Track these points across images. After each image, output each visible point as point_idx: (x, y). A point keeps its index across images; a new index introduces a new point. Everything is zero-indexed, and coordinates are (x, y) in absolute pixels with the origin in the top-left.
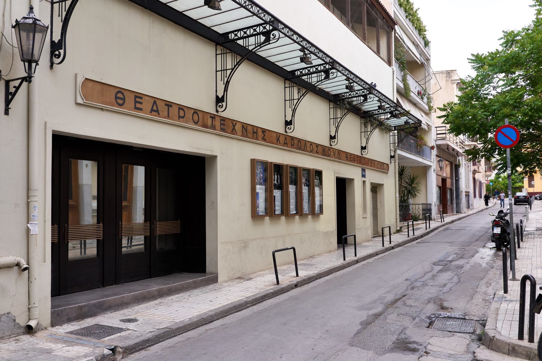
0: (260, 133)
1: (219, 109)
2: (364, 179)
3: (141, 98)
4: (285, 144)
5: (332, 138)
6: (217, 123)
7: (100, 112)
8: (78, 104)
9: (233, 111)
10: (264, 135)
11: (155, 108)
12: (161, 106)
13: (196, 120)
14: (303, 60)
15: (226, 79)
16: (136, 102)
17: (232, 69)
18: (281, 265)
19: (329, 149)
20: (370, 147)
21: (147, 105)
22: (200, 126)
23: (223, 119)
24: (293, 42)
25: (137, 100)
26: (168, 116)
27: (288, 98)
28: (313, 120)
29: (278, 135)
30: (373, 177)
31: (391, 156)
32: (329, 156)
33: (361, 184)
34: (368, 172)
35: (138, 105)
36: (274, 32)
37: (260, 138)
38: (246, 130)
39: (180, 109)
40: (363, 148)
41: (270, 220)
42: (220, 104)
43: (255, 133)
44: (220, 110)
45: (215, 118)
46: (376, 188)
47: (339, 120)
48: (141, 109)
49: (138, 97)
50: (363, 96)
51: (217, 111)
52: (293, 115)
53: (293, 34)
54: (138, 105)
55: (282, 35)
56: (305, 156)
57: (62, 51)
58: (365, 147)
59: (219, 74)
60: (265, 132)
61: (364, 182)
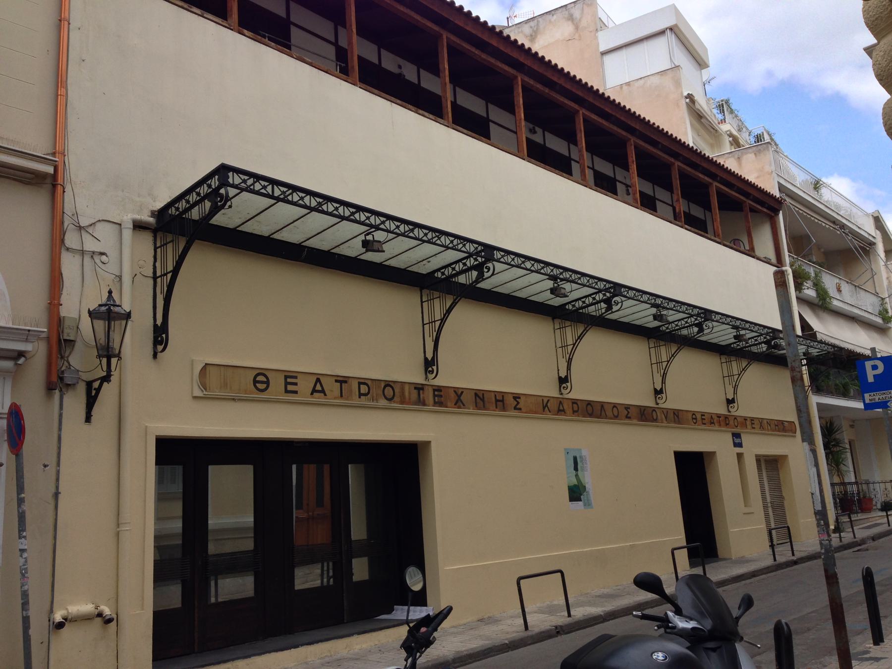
0: (510, 401)
1: (659, 401)
2: (739, 450)
5: (658, 392)
6: (429, 395)
7: (232, 403)
8: (195, 398)
9: (672, 401)
10: (518, 403)
11: (561, 408)
12: (328, 384)
13: (590, 412)
14: (656, 317)
15: (662, 372)
16: (287, 384)
17: (442, 320)
19: (654, 410)
20: (740, 397)
21: (304, 386)
22: (397, 403)
23: (438, 390)
24: (274, 201)
25: (289, 380)
26: (341, 396)
27: (654, 361)
28: (694, 382)
29: (545, 400)
30: (757, 445)
31: (560, 378)
32: (655, 420)
34: (745, 439)
35: (290, 388)
36: (615, 299)
39: (573, 403)
40: (730, 402)
42: (564, 385)
43: (499, 401)
44: (431, 376)
45: (422, 389)
46: (771, 465)
47: (736, 377)
49: (290, 379)
50: (696, 325)
51: (657, 404)
52: (663, 382)
53: (725, 318)
54: (290, 388)
55: (623, 299)
57: (435, 368)
58: (733, 399)
59: (655, 366)
60: (519, 398)
61: (740, 456)
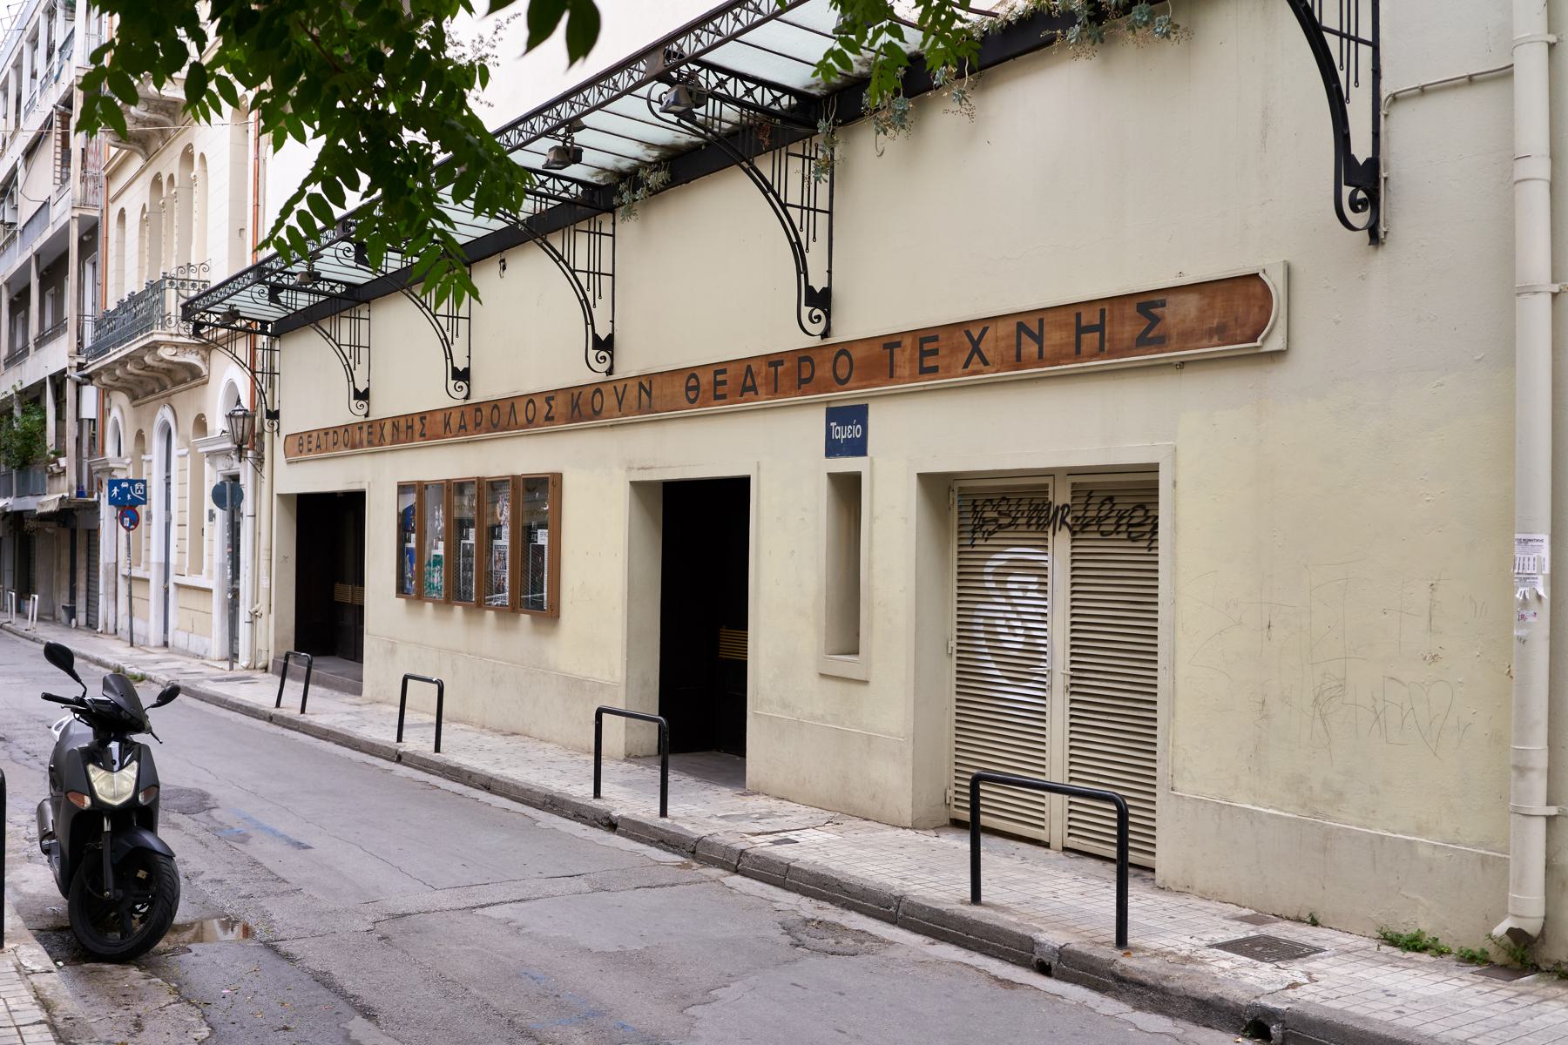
3: (935, 339)
4: (463, 428)
16: (924, 354)
18: (451, 721)
32: (596, 414)
33: (817, 500)
35: (930, 362)
37: (417, 435)
38: (649, 394)
41: (533, 619)
48: (934, 370)
56: (518, 441)
61: (848, 490)
